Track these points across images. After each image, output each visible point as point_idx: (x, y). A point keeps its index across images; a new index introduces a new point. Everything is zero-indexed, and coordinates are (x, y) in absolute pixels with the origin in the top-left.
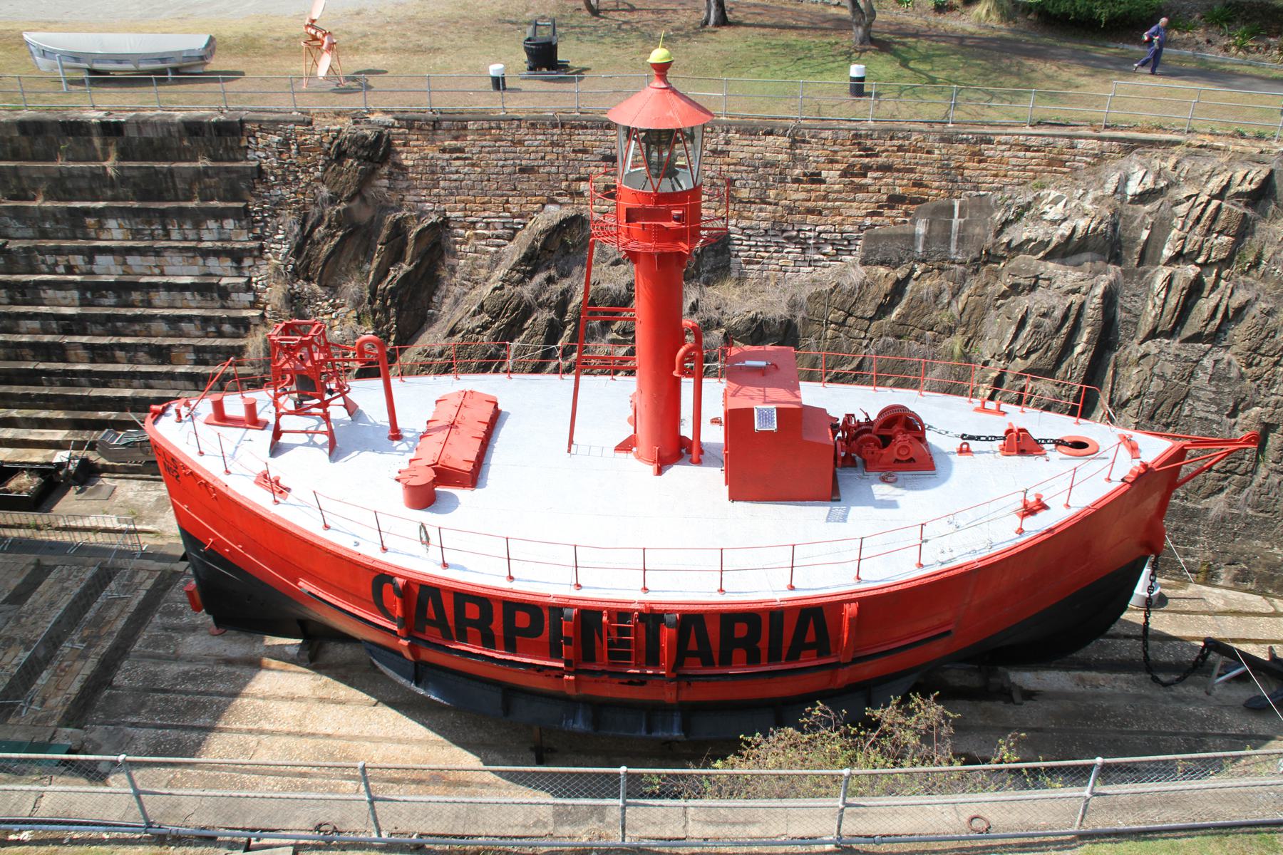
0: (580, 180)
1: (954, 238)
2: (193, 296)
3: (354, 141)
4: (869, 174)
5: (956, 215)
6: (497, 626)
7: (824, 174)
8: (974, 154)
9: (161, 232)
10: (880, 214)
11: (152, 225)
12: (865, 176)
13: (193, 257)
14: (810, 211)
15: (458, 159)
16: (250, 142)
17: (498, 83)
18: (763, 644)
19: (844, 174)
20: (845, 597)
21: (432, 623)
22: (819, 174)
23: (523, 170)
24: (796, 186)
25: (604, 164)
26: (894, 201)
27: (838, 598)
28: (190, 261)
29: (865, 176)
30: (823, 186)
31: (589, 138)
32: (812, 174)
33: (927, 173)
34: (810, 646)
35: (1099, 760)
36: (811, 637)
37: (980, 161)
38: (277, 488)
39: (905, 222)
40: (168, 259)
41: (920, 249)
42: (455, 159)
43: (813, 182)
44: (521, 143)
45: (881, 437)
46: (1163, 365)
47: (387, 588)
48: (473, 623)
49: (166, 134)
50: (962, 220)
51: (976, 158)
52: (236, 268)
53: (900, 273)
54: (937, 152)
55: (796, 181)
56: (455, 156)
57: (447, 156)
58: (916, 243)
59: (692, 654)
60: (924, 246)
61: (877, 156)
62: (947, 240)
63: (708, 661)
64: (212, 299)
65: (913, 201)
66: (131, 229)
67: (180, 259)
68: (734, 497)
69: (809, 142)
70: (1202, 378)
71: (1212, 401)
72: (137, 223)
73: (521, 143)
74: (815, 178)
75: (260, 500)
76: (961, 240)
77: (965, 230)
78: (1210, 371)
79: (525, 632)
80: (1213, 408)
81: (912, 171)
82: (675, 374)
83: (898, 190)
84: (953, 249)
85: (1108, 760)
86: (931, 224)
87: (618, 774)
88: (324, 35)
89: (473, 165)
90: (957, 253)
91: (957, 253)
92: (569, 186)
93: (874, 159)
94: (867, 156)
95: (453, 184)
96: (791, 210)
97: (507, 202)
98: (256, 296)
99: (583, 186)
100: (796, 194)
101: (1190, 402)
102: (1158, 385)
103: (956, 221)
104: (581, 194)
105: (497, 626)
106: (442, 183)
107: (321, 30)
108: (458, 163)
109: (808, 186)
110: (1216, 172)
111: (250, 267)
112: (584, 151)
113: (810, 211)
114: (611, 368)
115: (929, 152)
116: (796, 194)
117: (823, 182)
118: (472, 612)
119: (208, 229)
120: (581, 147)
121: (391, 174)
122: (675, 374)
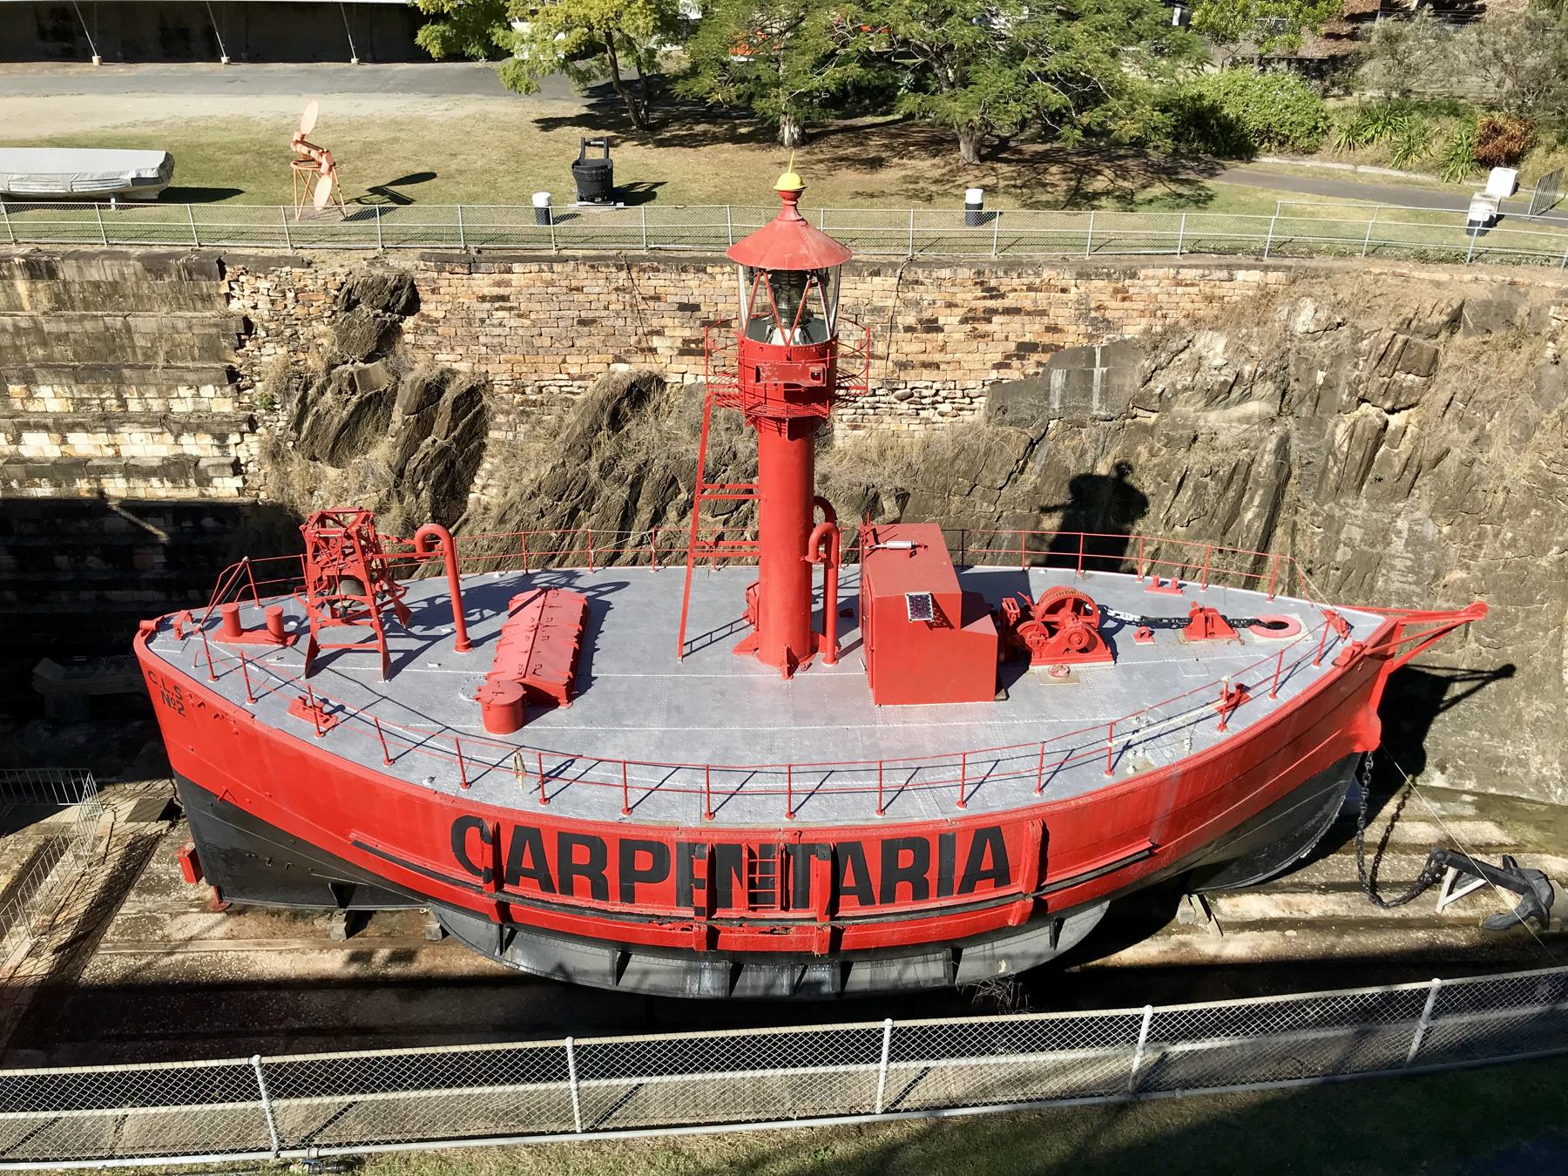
0: (652, 333)
1: (1096, 390)
2: (162, 482)
3: (367, 287)
4: (995, 319)
5: (1098, 363)
6: (612, 873)
7: (941, 321)
8: (1116, 291)
9: (114, 402)
10: (1008, 366)
11: (102, 392)
12: (990, 322)
13: (161, 433)
14: (925, 365)
15: (503, 309)
16: (231, 289)
17: (545, 215)
18: (932, 875)
19: (964, 321)
20: (1025, 814)
21: (529, 874)
22: (936, 320)
23: (582, 322)
24: (909, 335)
25: (680, 314)
26: (1025, 349)
27: (1019, 816)
28: (156, 438)
29: (990, 322)
30: (941, 335)
31: (662, 283)
32: (929, 321)
33: (1062, 315)
34: (986, 875)
35: (1436, 983)
36: (987, 864)
37: (1124, 299)
38: (325, 714)
39: (1037, 374)
40: (126, 436)
41: (1056, 405)
42: (497, 310)
43: (928, 330)
44: (579, 289)
45: (1047, 624)
46: (1349, 529)
47: (472, 833)
48: (581, 870)
49: (117, 278)
50: (1105, 369)
51: (1119, 296)
52: (218, 447)
53: (1031, 433)
54: (1073, 290)
55: (909, 329)
56: (497, 305)
57: (487, 305)
58: (1051, 398)
59: (849, 891)
60: (1062, 402)
61: (1003, 296)
62: (1088, 392)
63: (866, 900)
64: (188, 486)
65: (1046, 349)
66: (72, 399)
67: (142, 436)
68: (880, 701)
69: (922, 284)
70: (1398, 544)
71: (1411, 570)
72: (80, 391)
73: (579, 289)
74: (932, 326)
75: (301, 731)
76: (1105, 393)
77: (1107, 381)
78: (1405, 534)
79: (647, 877)
80: (1411, 578)
81: (1043, 313)
82: (809, 558)
83: (1028, 338)
84: (1096, 403)
85: (1448, 982)
86: (1067, 376)
87: (564, 1050)
88: (321, 154)
89: (520, 316)
90: (1099, 409)
91: (1099, 409)
92: (639, 342)
93: (999, 301)
94: (992, 297)
95: (496, 341)
96: (903, 366)
97: (564, 362)
98: (245, 481)
99: (656, 342)
100: (911, 347)
101: (1384, 571)
102: (1345, 553)
103: (1099, 371)
104: (653, 350)
105: (612, 873)
106: (482, 339)
107: (317, 148)
108: (501, 314)
109: (924, 336)
110: (1021, 242)
111: (236, 445)
112: (657, 298)
113: (925, 365)
114: (717, 552)
115: (1064, 291)
116: (911, 347)
117: (940, 330)
118: (581, 855)
119: (179, 397)
120: (652, 293)
121: (417, 327)
122: (809, 558)
